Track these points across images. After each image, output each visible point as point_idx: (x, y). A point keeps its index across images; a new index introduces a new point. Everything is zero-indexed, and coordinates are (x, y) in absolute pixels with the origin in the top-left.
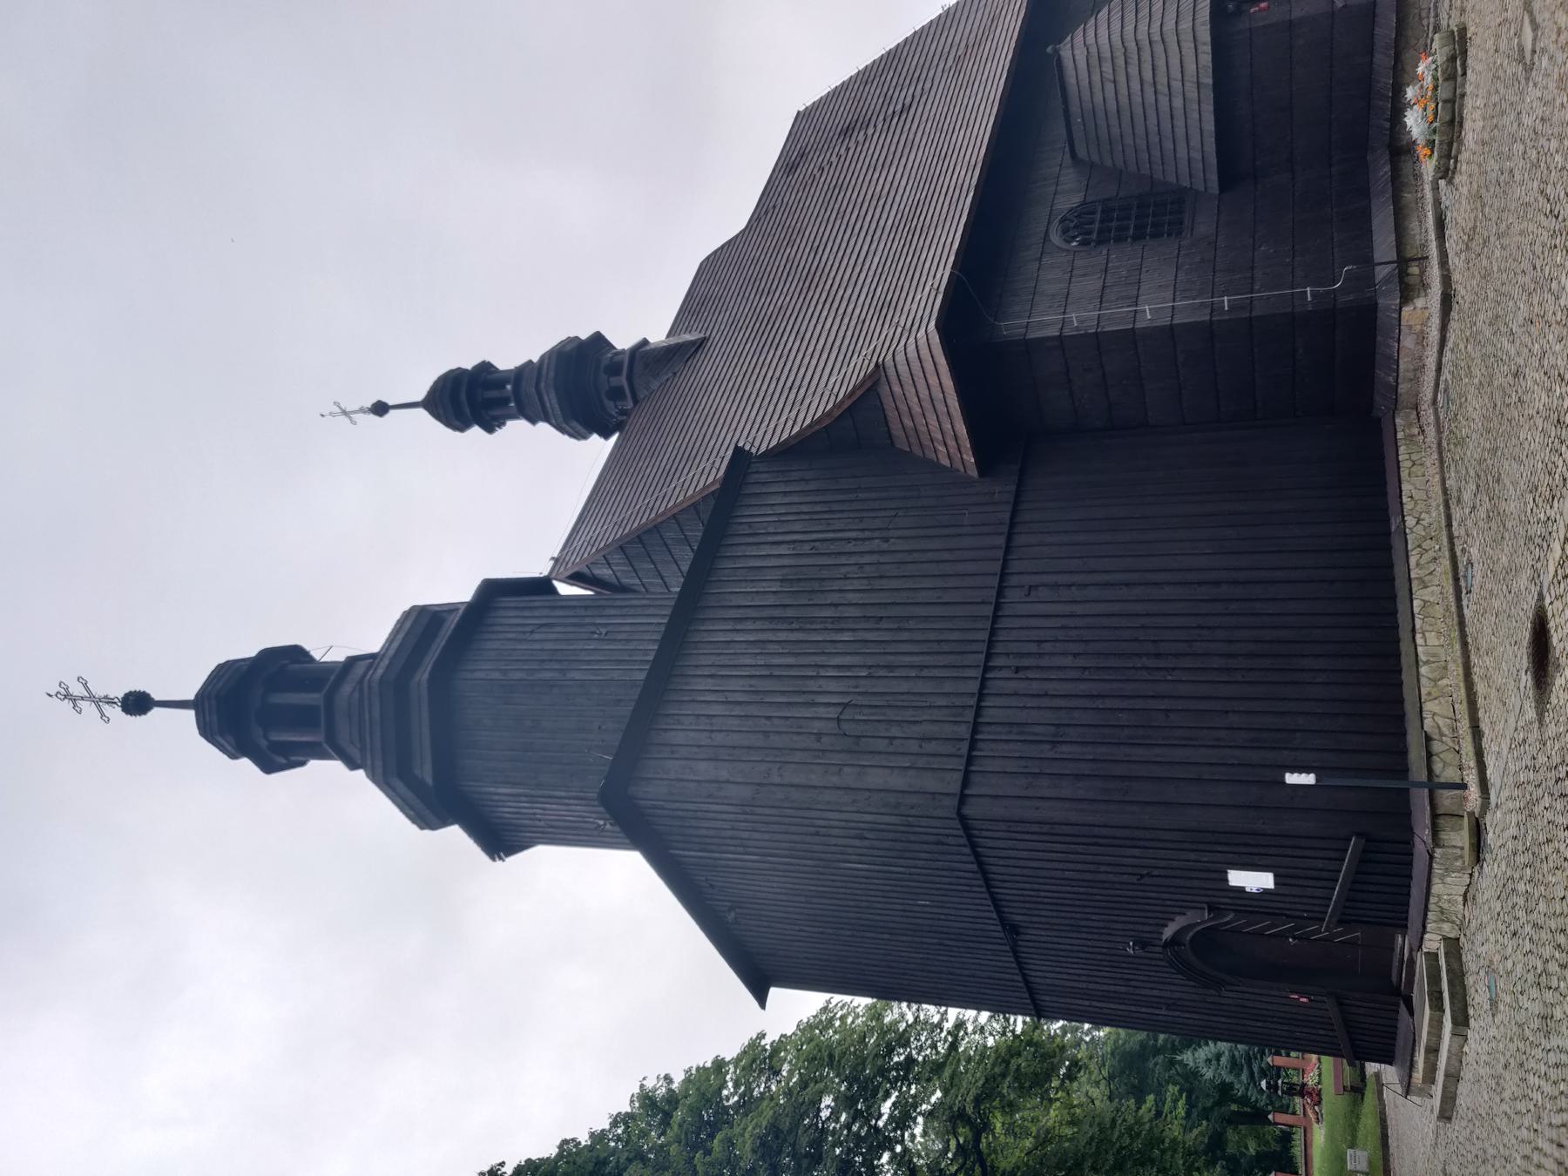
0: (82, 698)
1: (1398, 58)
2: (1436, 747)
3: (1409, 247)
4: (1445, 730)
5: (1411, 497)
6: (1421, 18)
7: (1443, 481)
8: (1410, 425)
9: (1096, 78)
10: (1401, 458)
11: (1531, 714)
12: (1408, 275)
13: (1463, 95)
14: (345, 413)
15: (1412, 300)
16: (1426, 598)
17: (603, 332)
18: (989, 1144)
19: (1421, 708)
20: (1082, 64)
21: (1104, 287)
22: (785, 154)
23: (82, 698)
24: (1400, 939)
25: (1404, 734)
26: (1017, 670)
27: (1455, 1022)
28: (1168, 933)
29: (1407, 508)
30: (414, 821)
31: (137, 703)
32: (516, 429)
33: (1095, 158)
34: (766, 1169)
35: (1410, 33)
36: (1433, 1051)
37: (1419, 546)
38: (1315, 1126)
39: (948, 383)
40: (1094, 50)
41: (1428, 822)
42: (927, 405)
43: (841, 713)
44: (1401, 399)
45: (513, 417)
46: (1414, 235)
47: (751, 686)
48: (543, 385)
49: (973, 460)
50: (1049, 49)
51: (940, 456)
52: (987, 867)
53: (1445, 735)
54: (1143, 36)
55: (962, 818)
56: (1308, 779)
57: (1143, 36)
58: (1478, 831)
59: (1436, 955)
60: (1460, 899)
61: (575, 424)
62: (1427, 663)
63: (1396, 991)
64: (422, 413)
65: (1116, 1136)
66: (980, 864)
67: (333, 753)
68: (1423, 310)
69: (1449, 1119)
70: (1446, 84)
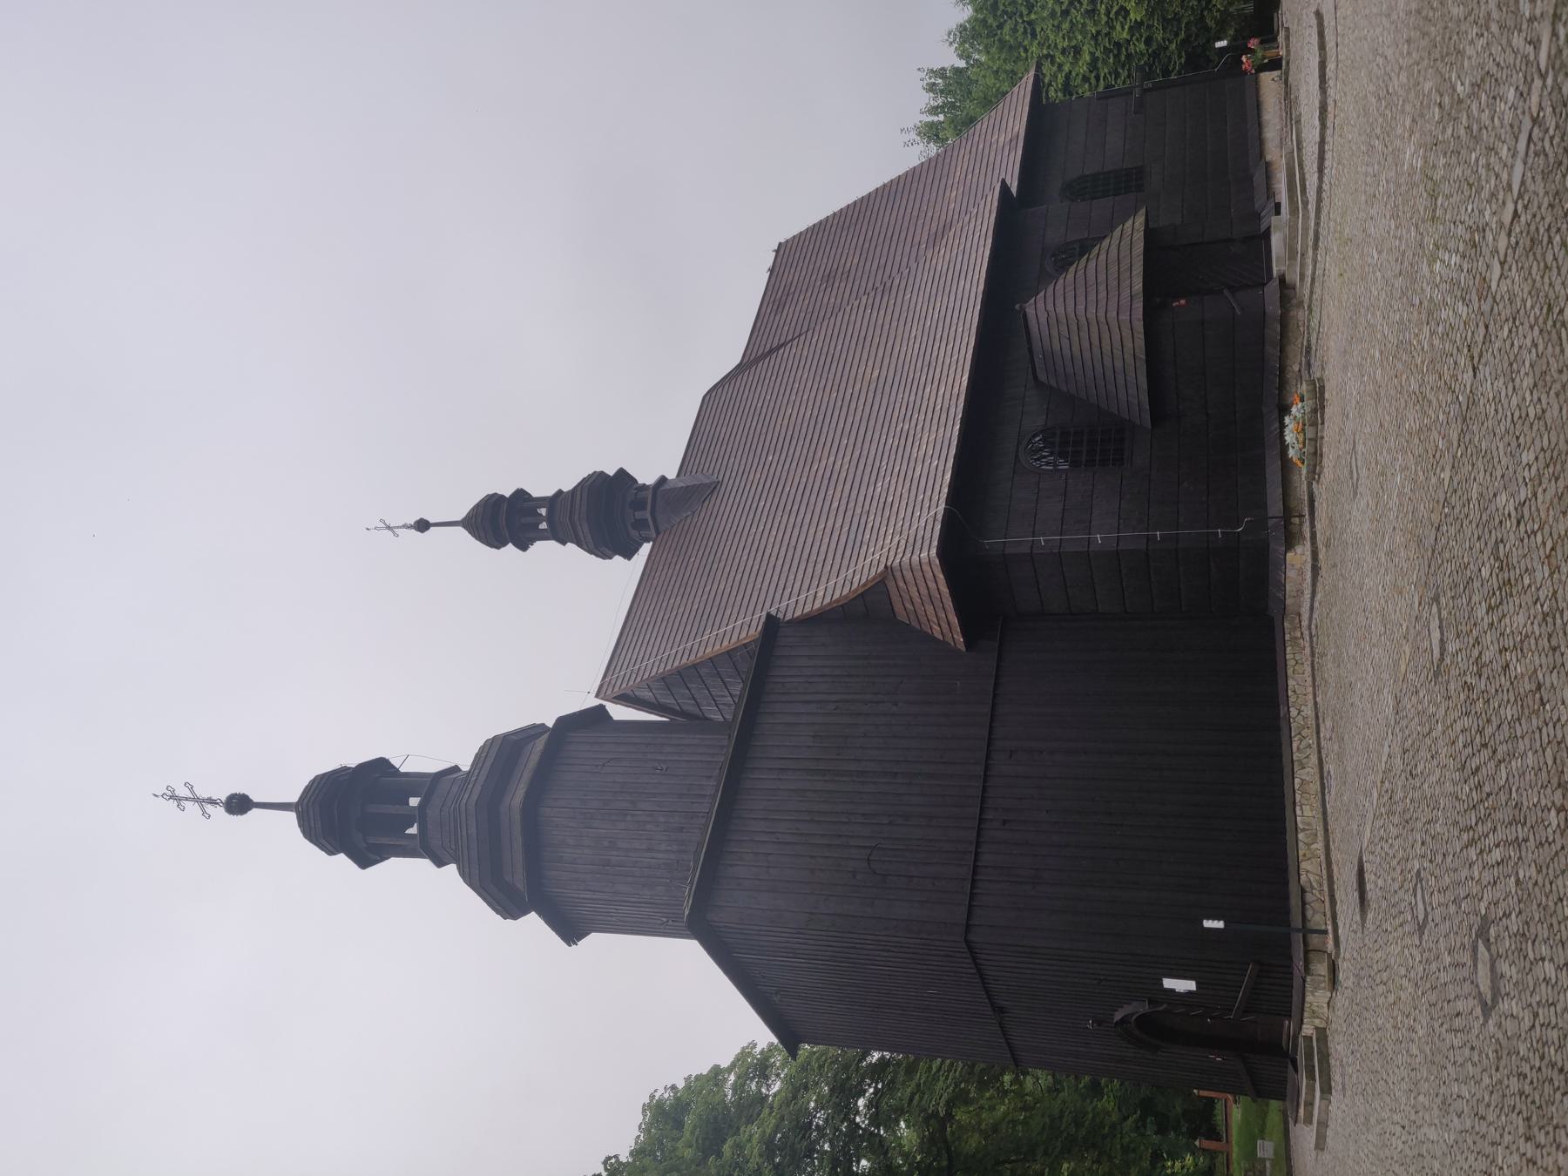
0: (187, 799)
1: (1282, 350)
2: (1309, 897)
3: (1292, 498)
4: (1315, 884)
5: (1294, 691)
6: (1298, 326)
7: (1315, 696)
8: (1295, 629)
9: (1055, 333)
10: (1287, 657)
11: (1357, 918)
12: (1291, 523)
13: (1322, 438)
14: (389, 528)
15: (1294, 547)
16: (1303, 777)
17: (624, 468)
18: (953, 1133)
19: (1299, 866)
20: (1043, 320)
21: (1064, 510)
22: (770, 288)
23: (187, 799)
24: (1287, 1022)
25: (1287, 883)
26: (1005, 822)
27: (1322, 1091)
28: (1118, 1016)
29: (1292, 700)
30: (497, 912)
31: (239, 804)
32: (544, 549)
33: (1053, 383)
34: (770, 1171)
35: (1290, 334)
36: (1310, 1104)
37: (1300, 734)
38: (1234, 1106)
39: (945, 590)
40: (1052, 314)
41: (1302, 955)
42: (926, 598)
43: (870, 855)
44: (1287, 608)
45: (544, 536)
46: (1296, 487)
47: (798, 829)
48: (576, 517)
49: (962, 640)
50: (1017, 307)
51: (934, 632)
52: (973, 944)
53: (1315, 889)
54: (1091, 316)
55: (967, 941)
56: (1220, 924)
57: (1091, 316)
58: (1333, 969)
59: (1311, 1038)
60: (1326, 1005)
61: (603, 549)
62: (1303, 830)
63: (1285, 1054)
64: (461, 531)
65: (1064, 1126)
66: (979, 970)
67: (423, 853)
68: (1298, 557)
69: (1323, 1149)
70: (1311, 428)
